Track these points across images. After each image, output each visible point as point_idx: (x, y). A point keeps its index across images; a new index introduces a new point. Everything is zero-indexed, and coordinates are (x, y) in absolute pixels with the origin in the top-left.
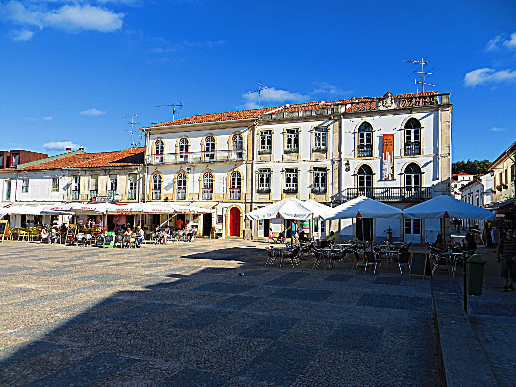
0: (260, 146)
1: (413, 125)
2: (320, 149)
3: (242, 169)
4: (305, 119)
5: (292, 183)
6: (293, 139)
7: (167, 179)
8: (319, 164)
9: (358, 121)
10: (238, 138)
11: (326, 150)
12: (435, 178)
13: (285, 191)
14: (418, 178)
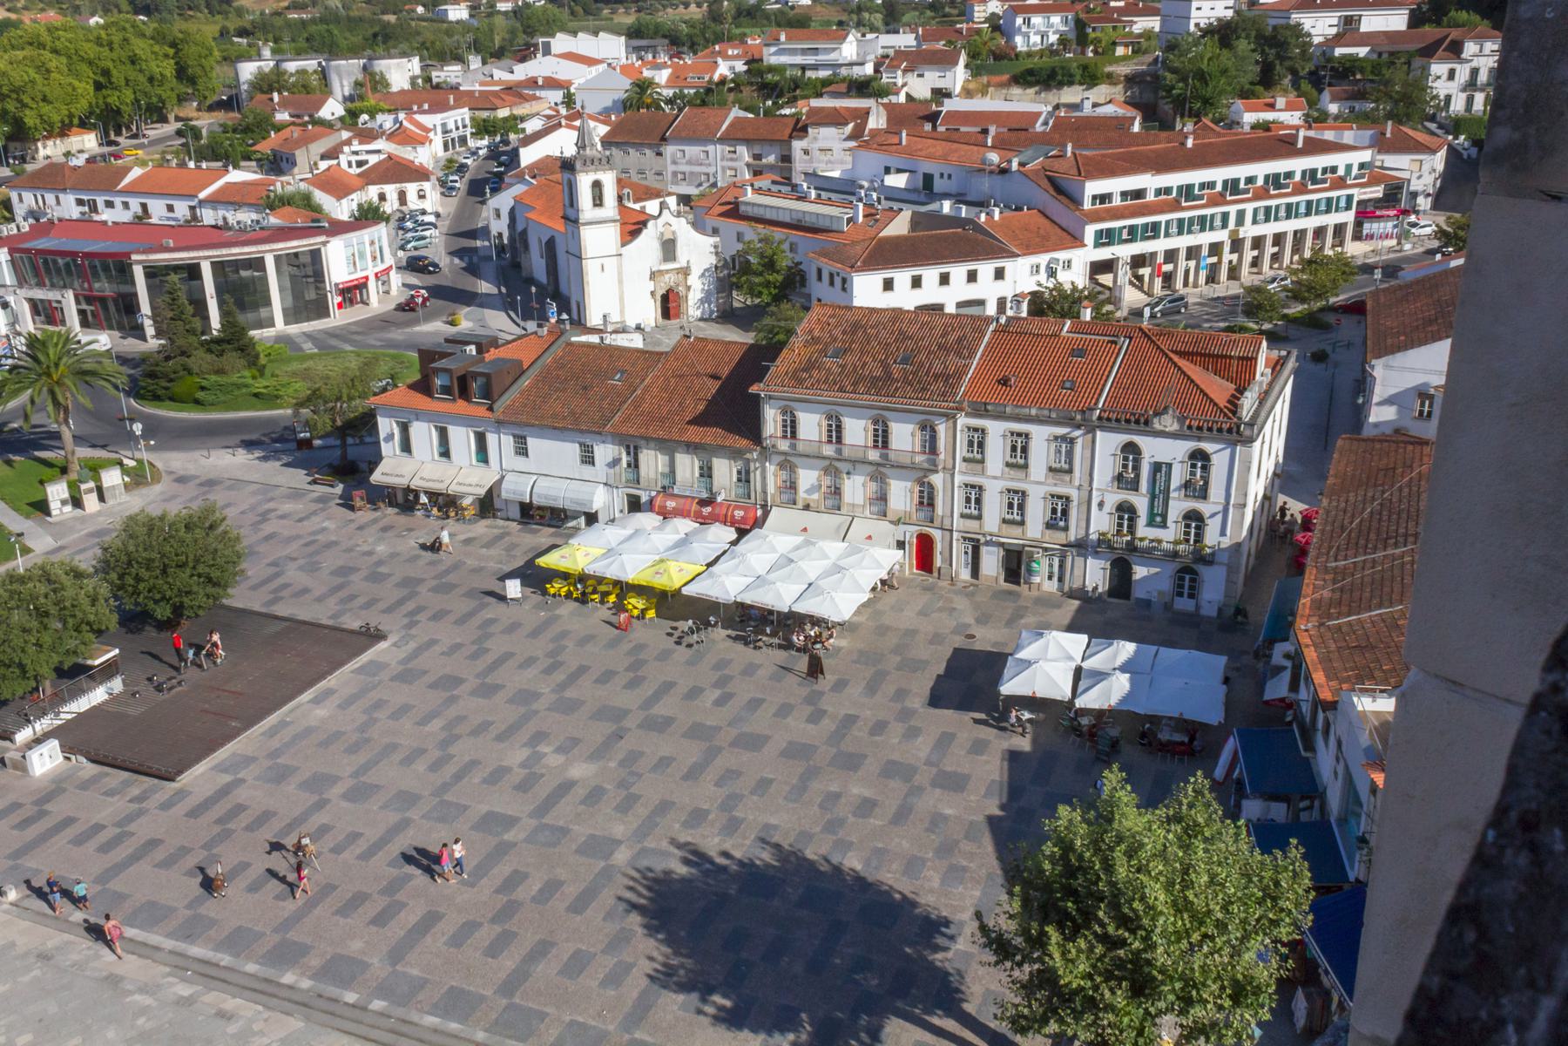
0: (965, 448)
3: (937, 480)
4: (1000, 416)
6: (1020, 448)
7: (807, 478)
10: (928, 430)
11: (1070, 471)
13: (1004, 521)
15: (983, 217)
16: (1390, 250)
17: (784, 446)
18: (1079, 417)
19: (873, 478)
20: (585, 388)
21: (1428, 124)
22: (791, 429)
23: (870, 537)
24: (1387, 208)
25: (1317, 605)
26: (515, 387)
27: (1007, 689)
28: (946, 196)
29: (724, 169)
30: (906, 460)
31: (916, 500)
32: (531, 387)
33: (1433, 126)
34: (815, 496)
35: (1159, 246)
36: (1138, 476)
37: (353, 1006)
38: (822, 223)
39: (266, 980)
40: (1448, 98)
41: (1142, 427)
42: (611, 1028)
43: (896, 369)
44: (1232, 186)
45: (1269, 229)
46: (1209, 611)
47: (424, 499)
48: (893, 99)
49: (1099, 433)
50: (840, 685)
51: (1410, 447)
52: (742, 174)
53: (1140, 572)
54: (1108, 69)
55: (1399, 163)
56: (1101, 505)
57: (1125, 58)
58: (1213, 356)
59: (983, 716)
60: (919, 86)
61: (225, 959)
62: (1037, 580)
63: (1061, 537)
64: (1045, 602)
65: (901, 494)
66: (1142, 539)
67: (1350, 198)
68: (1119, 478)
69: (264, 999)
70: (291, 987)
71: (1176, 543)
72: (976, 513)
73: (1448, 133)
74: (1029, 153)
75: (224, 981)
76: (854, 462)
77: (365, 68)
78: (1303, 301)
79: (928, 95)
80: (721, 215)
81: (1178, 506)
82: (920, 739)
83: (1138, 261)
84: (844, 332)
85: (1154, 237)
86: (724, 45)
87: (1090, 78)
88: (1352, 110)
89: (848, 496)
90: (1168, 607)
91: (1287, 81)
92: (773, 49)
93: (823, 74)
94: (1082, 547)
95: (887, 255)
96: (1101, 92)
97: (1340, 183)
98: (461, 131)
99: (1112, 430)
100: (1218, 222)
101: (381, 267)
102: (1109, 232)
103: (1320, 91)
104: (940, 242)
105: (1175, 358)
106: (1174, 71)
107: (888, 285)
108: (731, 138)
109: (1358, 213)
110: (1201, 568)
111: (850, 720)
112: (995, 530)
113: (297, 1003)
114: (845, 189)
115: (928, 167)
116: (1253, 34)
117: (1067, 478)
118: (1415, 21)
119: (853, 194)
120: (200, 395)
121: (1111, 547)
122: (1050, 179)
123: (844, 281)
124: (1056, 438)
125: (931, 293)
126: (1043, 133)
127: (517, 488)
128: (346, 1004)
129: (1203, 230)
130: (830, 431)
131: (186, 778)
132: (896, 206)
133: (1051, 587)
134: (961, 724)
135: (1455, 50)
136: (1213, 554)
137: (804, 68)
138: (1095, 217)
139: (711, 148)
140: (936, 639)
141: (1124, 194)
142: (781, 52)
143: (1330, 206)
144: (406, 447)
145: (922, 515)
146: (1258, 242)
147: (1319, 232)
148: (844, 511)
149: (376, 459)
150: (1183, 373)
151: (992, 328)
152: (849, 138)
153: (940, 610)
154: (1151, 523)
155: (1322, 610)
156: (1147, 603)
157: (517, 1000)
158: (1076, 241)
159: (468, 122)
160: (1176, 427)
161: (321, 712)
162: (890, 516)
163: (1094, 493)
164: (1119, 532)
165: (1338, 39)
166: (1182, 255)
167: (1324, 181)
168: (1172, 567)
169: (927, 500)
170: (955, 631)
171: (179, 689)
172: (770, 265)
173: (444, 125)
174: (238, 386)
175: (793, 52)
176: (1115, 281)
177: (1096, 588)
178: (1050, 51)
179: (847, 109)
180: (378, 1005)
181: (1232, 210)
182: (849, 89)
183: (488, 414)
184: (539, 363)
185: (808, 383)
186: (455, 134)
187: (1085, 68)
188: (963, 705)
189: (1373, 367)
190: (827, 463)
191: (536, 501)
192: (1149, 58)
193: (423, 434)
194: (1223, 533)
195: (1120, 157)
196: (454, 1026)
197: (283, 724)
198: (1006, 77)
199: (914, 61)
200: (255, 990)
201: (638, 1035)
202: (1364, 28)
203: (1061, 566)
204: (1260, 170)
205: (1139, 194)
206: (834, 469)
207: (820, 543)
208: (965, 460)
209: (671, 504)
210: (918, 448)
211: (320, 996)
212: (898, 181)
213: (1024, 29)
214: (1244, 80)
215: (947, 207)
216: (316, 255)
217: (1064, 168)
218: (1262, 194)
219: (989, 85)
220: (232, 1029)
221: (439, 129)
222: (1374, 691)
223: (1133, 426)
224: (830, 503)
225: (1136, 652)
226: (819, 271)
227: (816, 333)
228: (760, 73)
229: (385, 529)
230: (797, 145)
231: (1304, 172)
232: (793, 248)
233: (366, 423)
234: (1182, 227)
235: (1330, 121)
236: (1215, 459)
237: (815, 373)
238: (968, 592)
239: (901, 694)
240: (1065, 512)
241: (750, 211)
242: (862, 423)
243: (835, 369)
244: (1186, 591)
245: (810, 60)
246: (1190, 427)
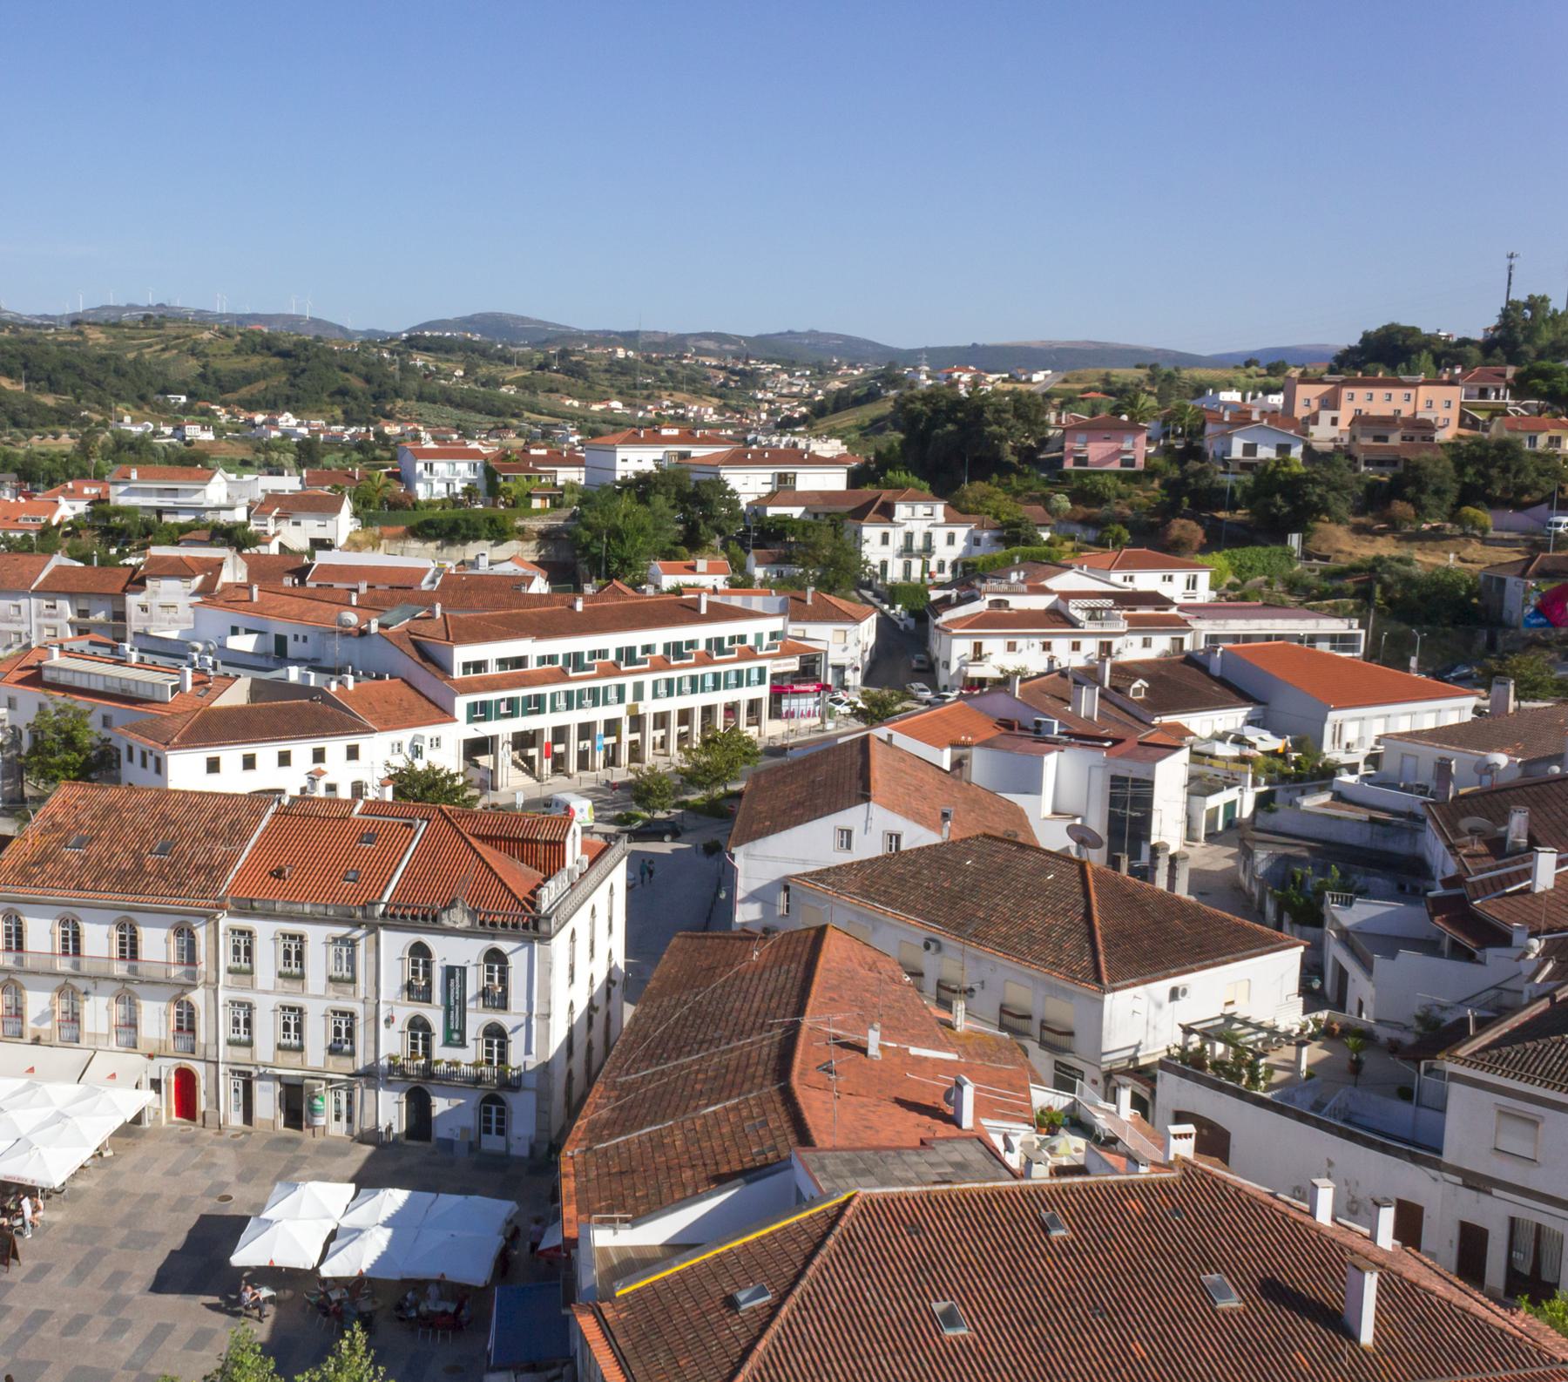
1: (495, 958)
2: (342, 981)
3: (198, 997)
4: (270, 915)
6: (295, 953)
8: (344, 1005)
9: (411, 938)
10: (185, 933)
11: (353, 981)
13: (280, 1047)
14: (503, 1046)
15: (334, 686)
16: (811, 730)
18: (359, 914)
19: (119, 999)
21: (864, 592)
23: (113, 1076)
24: (807, 682)
25: (592, 1127)
27: (240, 1258)
28: (297, 661)
30: (159, 974)
31: (173, 1025)
33: (868, 594)
34: (47, 1026)
35: (545, 722)
36: (429, 984)
38: (142, 692)
40: (884, 565)
41: (430, 924)
43: (150, 862)
44: (627, 655)
45: (674, 705)
46: (520, 1149)
48: (263, 549)
49: (383, 933)
50: (41, 1271)
51: (738, 944)
52: (64, 632)
53: (440, 1105)
54: (519, 523)
55: (822, 635)
57: (539, 512)
58: (518, 840)
59: (215, 1300)
60: (295, 535)
63: (345, 1065)
64: (331, 1150)
65: (155, 1019)
66: (437, 1062)
67: (762, 671)
68: (409, 987)
71: (476, 1065)
72: (245, 1038)
73: (884, 602)
74: (396, 613)
76: (95, 978)
78: (701, 786)
79: (306, 545)
80: (21, 682)
81: (477, 1019)
82: (127, 1336)
83: (524, 741)
84: (94, 817)
85: (538, 712)
86: (79, 483)
87: (499, 533)
88: (780, 575)
90: (473, 1147)
91: (717, 541)
92: (122, 489)
93: (183, 519)
94: (371, 1076)
95: (212, 729)
96: (513, 547)
97: (750, 654)
99: (397, 928)
100: (612, 696)
102: (484, 705)
103: (748, 552)
104: (284, 715)
105: (476, 843)
106: (588, 528)
107: (213, 766)
108: (49, 591)
109: (773, 687)
110: (508, 1097)
111: (40, 1317)
112: (269, 1059)
114: (175, 652)
115: (279, 627)
116: (674, 490)
117: (350, 989)
118: (855, 479)
119: (185, 657)
121: (405, 1076)
122: (415, 643)
123: (158, 761)
124: (335, 940)
125: (267, 775)
126: (431, 591)
129: (595, 704)
130: (66, 940)
132: (232, 672)
133: (338, 1129)
134: (189, 1312)
135: (887, 513)
136: (520, 1077)
137: (160, 512)
138: (467, 688)
139: (23, 602)
140: (182, 1203)
141: (502, 663)
142: (131, 492)
143: (740, 680)
145: (181, 1044)
146: (661, 720)
147: (732, 709)
148: (84, 1042)
150: (482, 859)
151: (272, 810)
153: (195, 1167)
154: (448, 1042)
155: (597, 1132)
156: (448, 1144)
158: (446, 715)
162: (141, 1046)
163: (382, 1007)
164: (414, 1056)
165: (771, 498)
166: (574, 734)
167: (731, 651)
168: (476, 1096)
169: (186, 1024)
170: (208, 1194)
172: (70, 742)
176: (496, 764)
177: (390, 1128)
178: (453, 501)
179: (196, 559)
181: (629, 682)
182: (212, 537)
185: (38, 880)
187: (492, 521)
188: (193, 1287)
189: (733, 857)
190: (61, 981)
192: (566, 513)
194: (528, 1051)
195: (495, 620)
198: (402, 529)
199: (289, 507)
203: (350, 1102)
204: (659, 637)
205: (520, 662)
206: (71, 990)
207: (47, 1086)
210: (173, 958)
212: (245, 643)
213: (426, 475)
214: (665, 539)
215: (294, 674)
217: (431, 632)
218: (661, 665)
219: (381, 537)
222: (613, 1221)
223: (420, 923)
224: (66, 1033)
225: (408, 1203)
226: (130, 749)
227: (59, 819)
228: (106, 516)
230: (133, 600)
231: (709, 642)
232: (106, 722)
234: (571, 701)
235: (756, 586)
236: (513, 961)
237: (49, 867)
238: (236, 1143)
239: (118, 1277)
240: (350, 1032)
241: (63, 679)
242: (105, 929)
243: (76, 862)
245: (167, 502)
246: (482, 923)
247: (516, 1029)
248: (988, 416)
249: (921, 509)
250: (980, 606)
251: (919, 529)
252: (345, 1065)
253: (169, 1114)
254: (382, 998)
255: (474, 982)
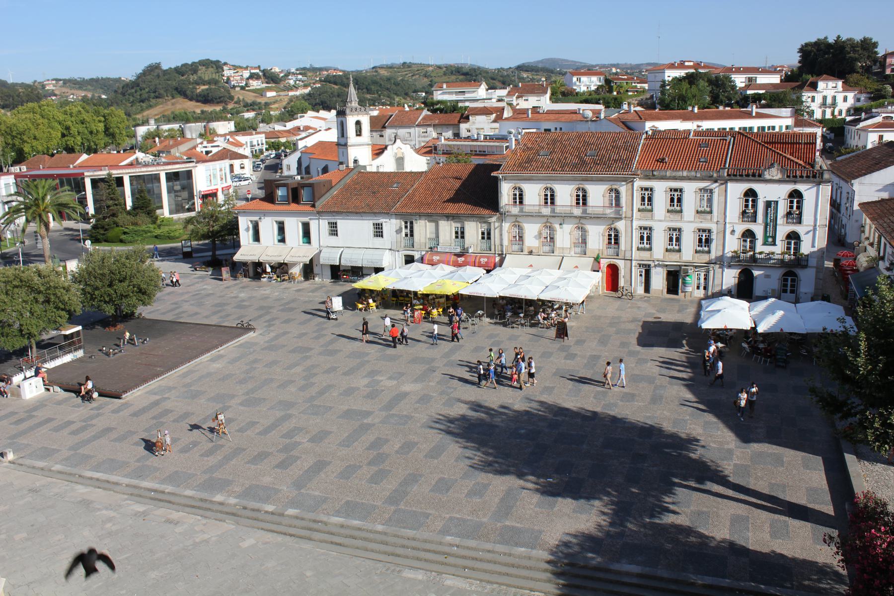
1: (796, 195)
3: (621, 225)
4: (689, 179)
5: (674, 242)
6: (676, 199)
7: (531, 230)
9: (745, 186)
11: (711, 212)
12: (813, 246)
13: (667, 250)
17: (515, 210)
20: (374, 193)
22: (519, 198)
26: (328, 194)
29: (419, 142)
32: (337, 195)
36: (755, 213)
37: (272, 513)
39: (201, 500)
41: (757, 178)
42: (485, 520)
47: (269, 270)
56: (733, 232)
61: (169, 488)
62: (689, 289)
65: (596, 235)
66: (761, 253)
69: (201, 512)
70: (221, 504)
71: (783, 253)
75: (170, 502)
77: (205, 127)
81: (783, 230)
89: (559, 242)
92: (439, 92)
94: (722, 262)
98: (260, 147)
101: (226, 185)
113: (227, 513)
117: (708, 216)
120: (123, 237)
124: (700, 190)
127: (330, 257)
128: (266, 512)
131: (128, 397)
137: (458, 101)
139: (412, 130)
144: (257, 238)
149: (237, 245)
152: (495, 121)
154: (765, 243)
157: (402, 506)
159: (264, 142)
160: (779, 176)
161: (217, 365)
163: (727, 225)
165: (748, 87)
169: (614, 239)
171: (120, 354)
173: (251, 142)
174: (146, 232)
175: (449, 93)
180: (291, 512)
183: (312, 209)
184: (342, 182)
186: (257, 148)
190: (544, 220)
191: (343, 263)
193: (268, 227)
196: (356, 523)
197: (190, 372)
200: (193, 507)
201: (507, 523)
202: (758, 81)
208: (639, 210)
209: (436, 258)
211: (245, 508)
213: (578, 83)
216: (189, 174)
220: (179, 529)
221: (249, 144)
229: (243, 288)
233: (233, 228)
244: (789, 288)
245: (461, 97)
247: (808, 233)
248: (848, 49)
249: (831, 84)
250: (878, 119)
251: (830, 94)
252: (705, 258)
253: (603, 290)
254: (727, 221)
255: (782, 209)
